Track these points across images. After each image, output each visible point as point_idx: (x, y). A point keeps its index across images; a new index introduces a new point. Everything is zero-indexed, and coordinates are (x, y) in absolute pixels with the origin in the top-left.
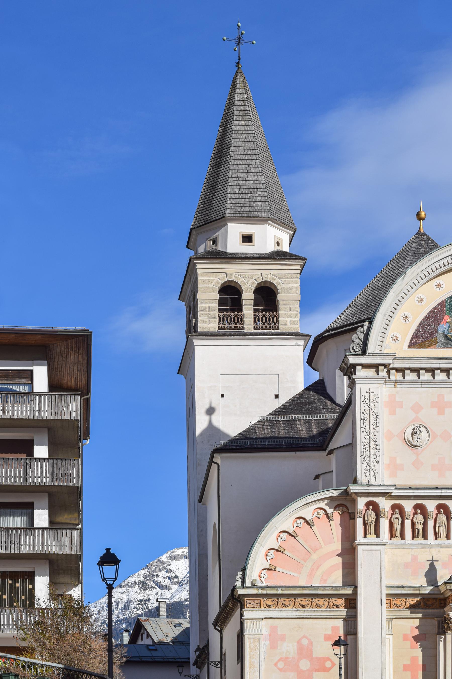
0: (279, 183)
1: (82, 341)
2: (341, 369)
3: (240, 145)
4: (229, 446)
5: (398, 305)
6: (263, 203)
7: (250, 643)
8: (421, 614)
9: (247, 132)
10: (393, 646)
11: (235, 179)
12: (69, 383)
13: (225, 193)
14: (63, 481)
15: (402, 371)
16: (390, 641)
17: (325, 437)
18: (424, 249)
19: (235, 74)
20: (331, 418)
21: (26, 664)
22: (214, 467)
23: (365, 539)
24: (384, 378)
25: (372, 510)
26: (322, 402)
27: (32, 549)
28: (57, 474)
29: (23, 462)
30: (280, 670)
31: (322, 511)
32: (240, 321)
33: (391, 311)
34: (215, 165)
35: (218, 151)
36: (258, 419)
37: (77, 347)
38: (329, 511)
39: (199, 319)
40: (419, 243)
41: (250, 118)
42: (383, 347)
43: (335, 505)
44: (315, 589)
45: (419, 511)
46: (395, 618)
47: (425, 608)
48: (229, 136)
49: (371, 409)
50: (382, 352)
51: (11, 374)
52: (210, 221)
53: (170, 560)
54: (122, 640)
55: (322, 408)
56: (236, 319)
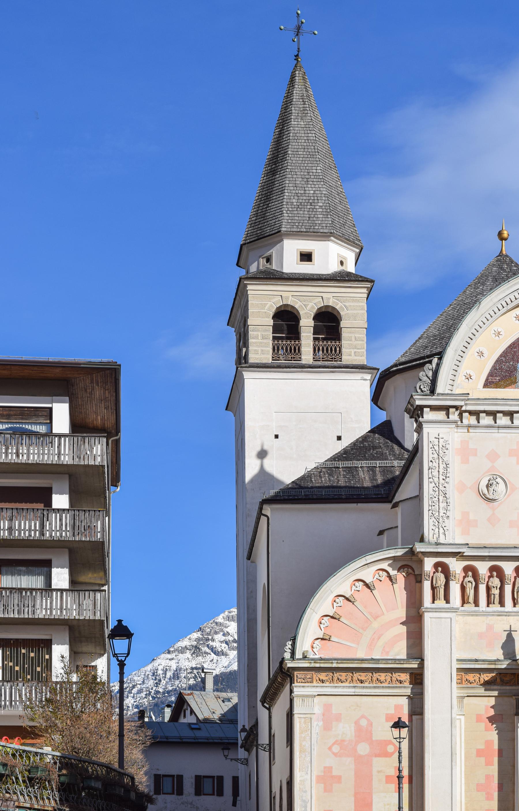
0: (344, 194)
1: (109, 375)
2: (407, 411)
3: (299, 150)
4: (280, 496)
5: (472, 339)
6: (325, 216)
7: (301, 724)
8: (497, 692)
9: (306, 135)
10: (465, 728)
11: (292, 188)
12: (95, 422)
13: (281, 204)
14: (86, 536)
15: (476, 414)
16: (461, 722)
17: (391, 487)
18: (506, 274)
19: (294, 69)
20: (398, 465)
21: (17, 752)
22: (263, 520)
23: (433, 606)
24: (456, 422)
25: (441, 572)
26: (388, 446)
27: (49, 613)
28: (79, 526)
29: (39, 513)
30: (335, 754)
31: (384, 572)
32: (297, 351)
33: (464, 346)
34: (270, 172)
35: (273, 156)
36: (313, 466)
37: (104, 381)
38: (393, 573)
39: (250, 348)
40: (501, 266)
41: (310, 118)
42: (454, 387)
43: (399, 566)
44: (374, 662)
45: (495, 574)
46: (468, 696)
47: (502, 685)
48: (286, 139)
49: (440, 457)
50: (453, 392)
51: (26, 412)
52: (263, 236)
53: (228, 622)
54: (163, 718)
55: (388, 453)
56: (293, 349)
